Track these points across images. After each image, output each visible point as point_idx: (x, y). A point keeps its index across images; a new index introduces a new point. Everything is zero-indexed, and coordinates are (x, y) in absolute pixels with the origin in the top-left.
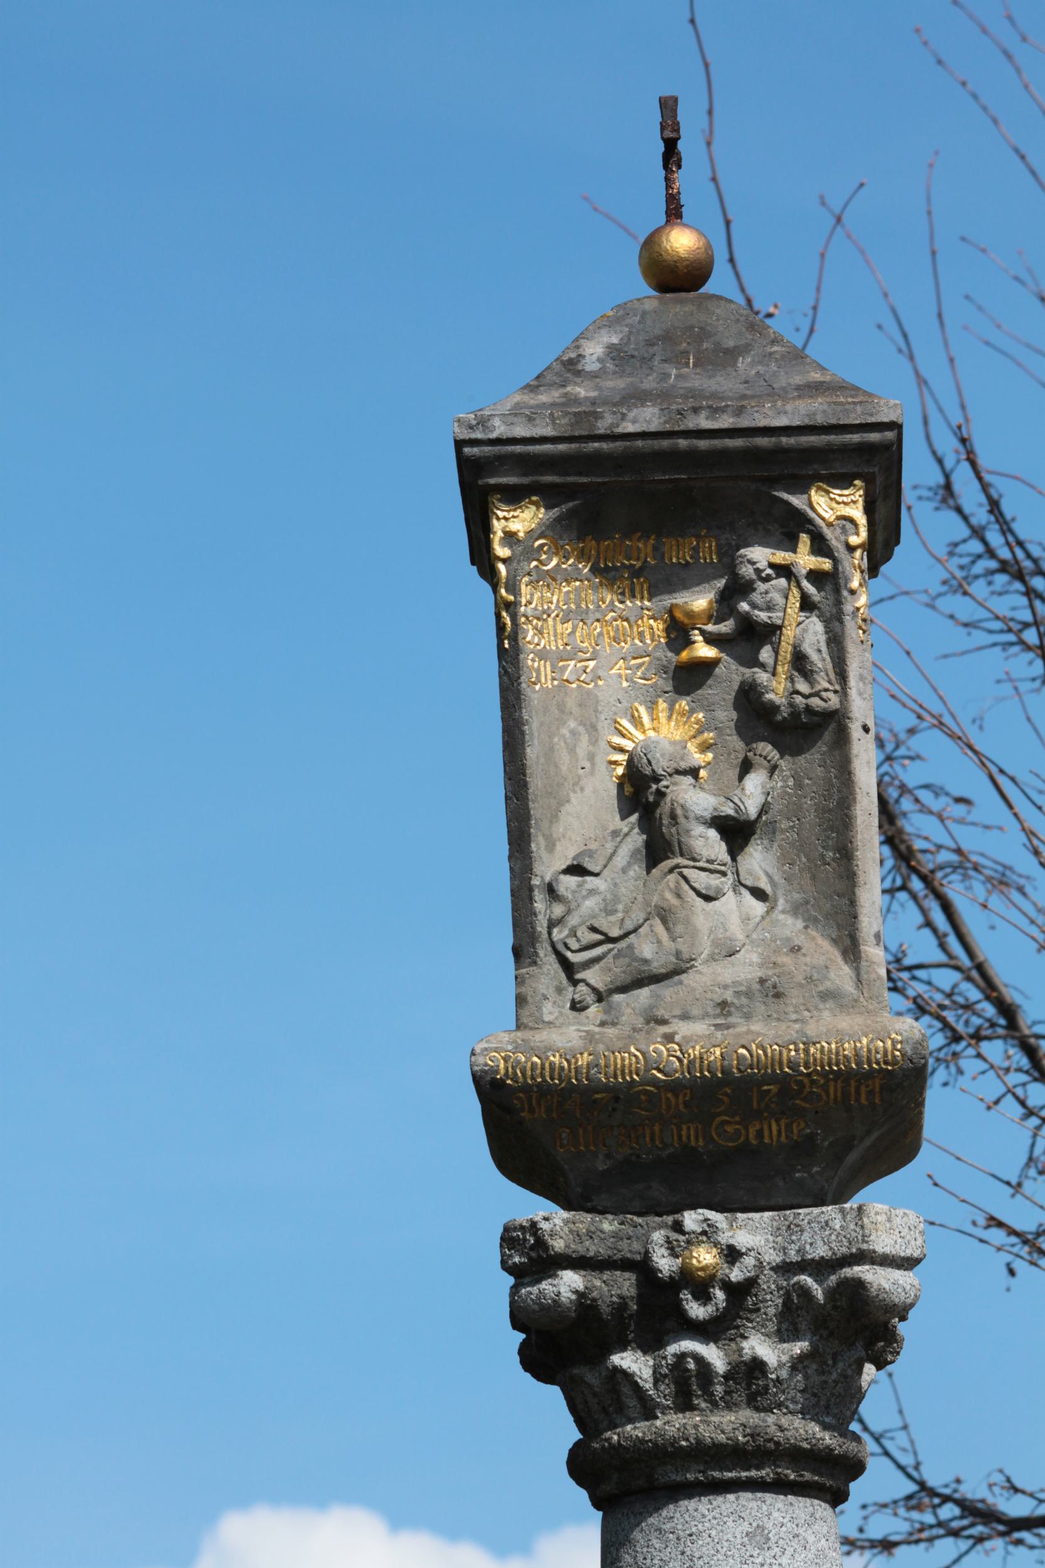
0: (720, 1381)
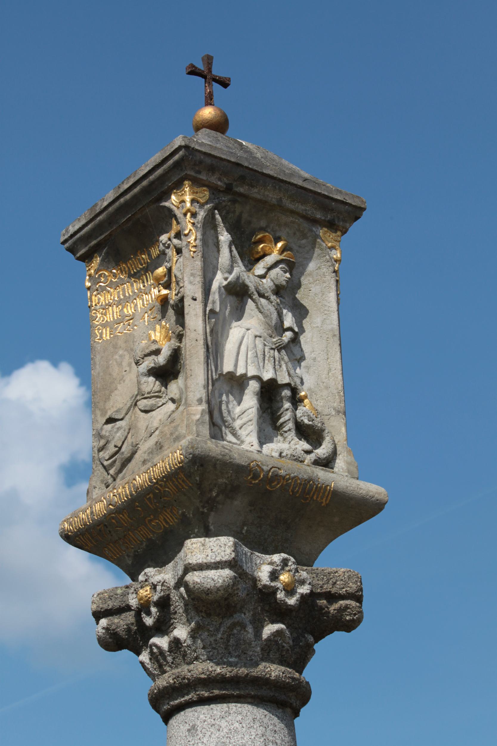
0: (168, 654)
